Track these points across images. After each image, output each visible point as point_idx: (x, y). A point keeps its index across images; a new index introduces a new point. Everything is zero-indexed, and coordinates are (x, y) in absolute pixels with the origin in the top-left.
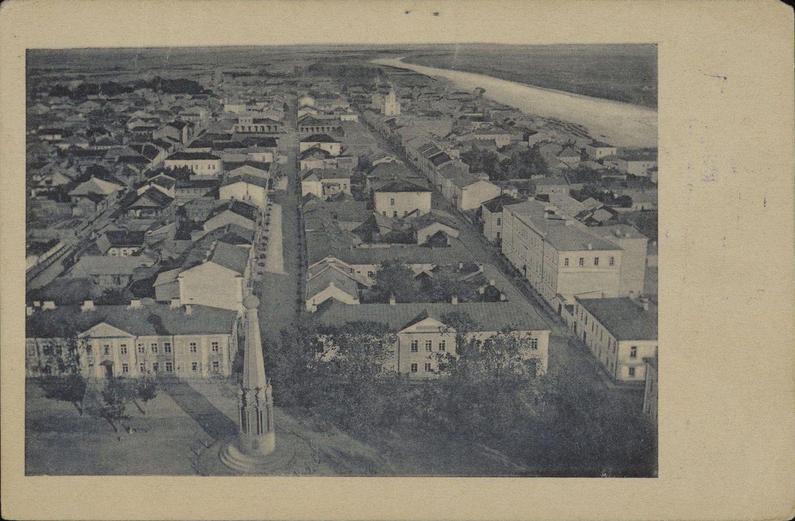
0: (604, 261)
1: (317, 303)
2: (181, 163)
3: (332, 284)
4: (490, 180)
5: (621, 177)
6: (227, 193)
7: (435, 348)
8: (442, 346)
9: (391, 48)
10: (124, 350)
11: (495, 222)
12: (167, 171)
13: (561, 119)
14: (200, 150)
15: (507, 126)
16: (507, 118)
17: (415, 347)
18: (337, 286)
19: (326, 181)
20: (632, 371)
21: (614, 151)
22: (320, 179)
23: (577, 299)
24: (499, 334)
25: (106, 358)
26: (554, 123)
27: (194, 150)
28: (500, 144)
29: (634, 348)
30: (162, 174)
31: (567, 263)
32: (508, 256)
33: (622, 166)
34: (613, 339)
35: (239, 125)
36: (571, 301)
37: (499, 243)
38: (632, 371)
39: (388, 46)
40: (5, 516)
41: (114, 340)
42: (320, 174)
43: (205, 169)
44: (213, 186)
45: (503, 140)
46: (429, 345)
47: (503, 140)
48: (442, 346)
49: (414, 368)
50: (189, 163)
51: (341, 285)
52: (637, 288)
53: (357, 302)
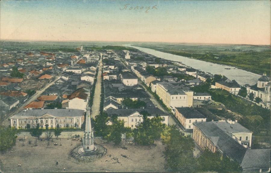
7: (138, 121)
8: (140, 120)
9: (171, 45)
10: (52, 122)
11: (154, 87)
13: (74, 42)
14: (76, 67)
19: (110, 76)
20: (190, 127)
21: (185, 69)
25: (47, 124)
27: (74, 67)
29: (190, 120)
31: (173, 98)
32: (63, 45)
35: (87, 61)
36: (174, 108)
39: (139, 42)
41: (49, 119)
42: (108, 74)
44: (80, 76)
45: (157, 66)
46: (136, 120)
49: (132, 126)
53: (117, 108)
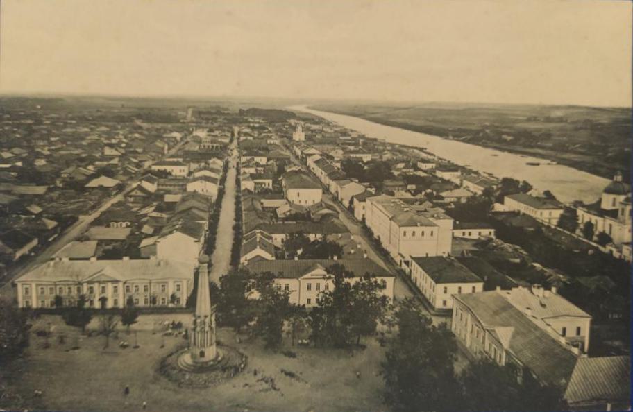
0: (409, 234)
1: (248, 259)
2: (162, 168)
3: (258, 247)
4: (359, 181)
5: (438, 181)
6: (191, 187)
7: (322, 288)
8: (327, 287)
12: (153, 173)
15: (371, 150)
16: (370, 144)
17: (309, 287)
18: (260, 248)
22: (253, 180)
23: (411, 257)
24: (361, 280)
26: (394, 149)
27: (171, 160)
28: (365, 160)
30: (150, 175)
33: (439, 174)
34: (433, 283)
35: (202, 145)
36: (408, 258)
37: (364, 219)
38: (445, 303)
40: (630, 2)
42: (253, 177)
43: (177, 171)
45: (367, 158)
46: (318, 287)
47: (367, 158)
48: (327, 287)
49: (309, 301)
50: (169, 168)
51: (265, 247)
52: (143, 255)
53: (274, 258)
